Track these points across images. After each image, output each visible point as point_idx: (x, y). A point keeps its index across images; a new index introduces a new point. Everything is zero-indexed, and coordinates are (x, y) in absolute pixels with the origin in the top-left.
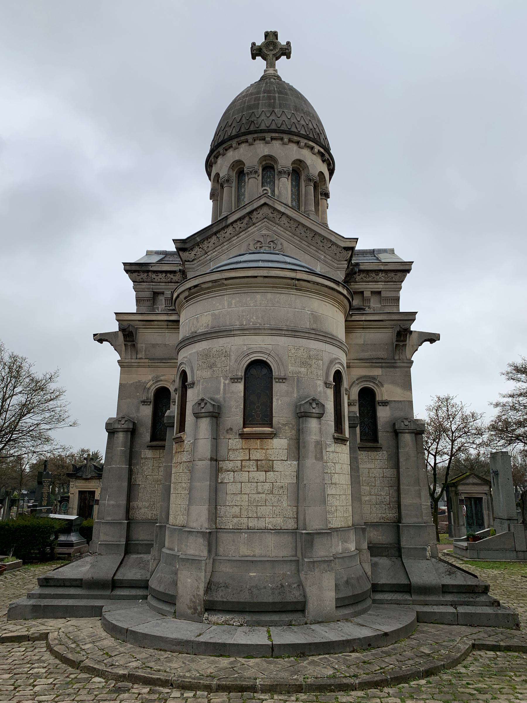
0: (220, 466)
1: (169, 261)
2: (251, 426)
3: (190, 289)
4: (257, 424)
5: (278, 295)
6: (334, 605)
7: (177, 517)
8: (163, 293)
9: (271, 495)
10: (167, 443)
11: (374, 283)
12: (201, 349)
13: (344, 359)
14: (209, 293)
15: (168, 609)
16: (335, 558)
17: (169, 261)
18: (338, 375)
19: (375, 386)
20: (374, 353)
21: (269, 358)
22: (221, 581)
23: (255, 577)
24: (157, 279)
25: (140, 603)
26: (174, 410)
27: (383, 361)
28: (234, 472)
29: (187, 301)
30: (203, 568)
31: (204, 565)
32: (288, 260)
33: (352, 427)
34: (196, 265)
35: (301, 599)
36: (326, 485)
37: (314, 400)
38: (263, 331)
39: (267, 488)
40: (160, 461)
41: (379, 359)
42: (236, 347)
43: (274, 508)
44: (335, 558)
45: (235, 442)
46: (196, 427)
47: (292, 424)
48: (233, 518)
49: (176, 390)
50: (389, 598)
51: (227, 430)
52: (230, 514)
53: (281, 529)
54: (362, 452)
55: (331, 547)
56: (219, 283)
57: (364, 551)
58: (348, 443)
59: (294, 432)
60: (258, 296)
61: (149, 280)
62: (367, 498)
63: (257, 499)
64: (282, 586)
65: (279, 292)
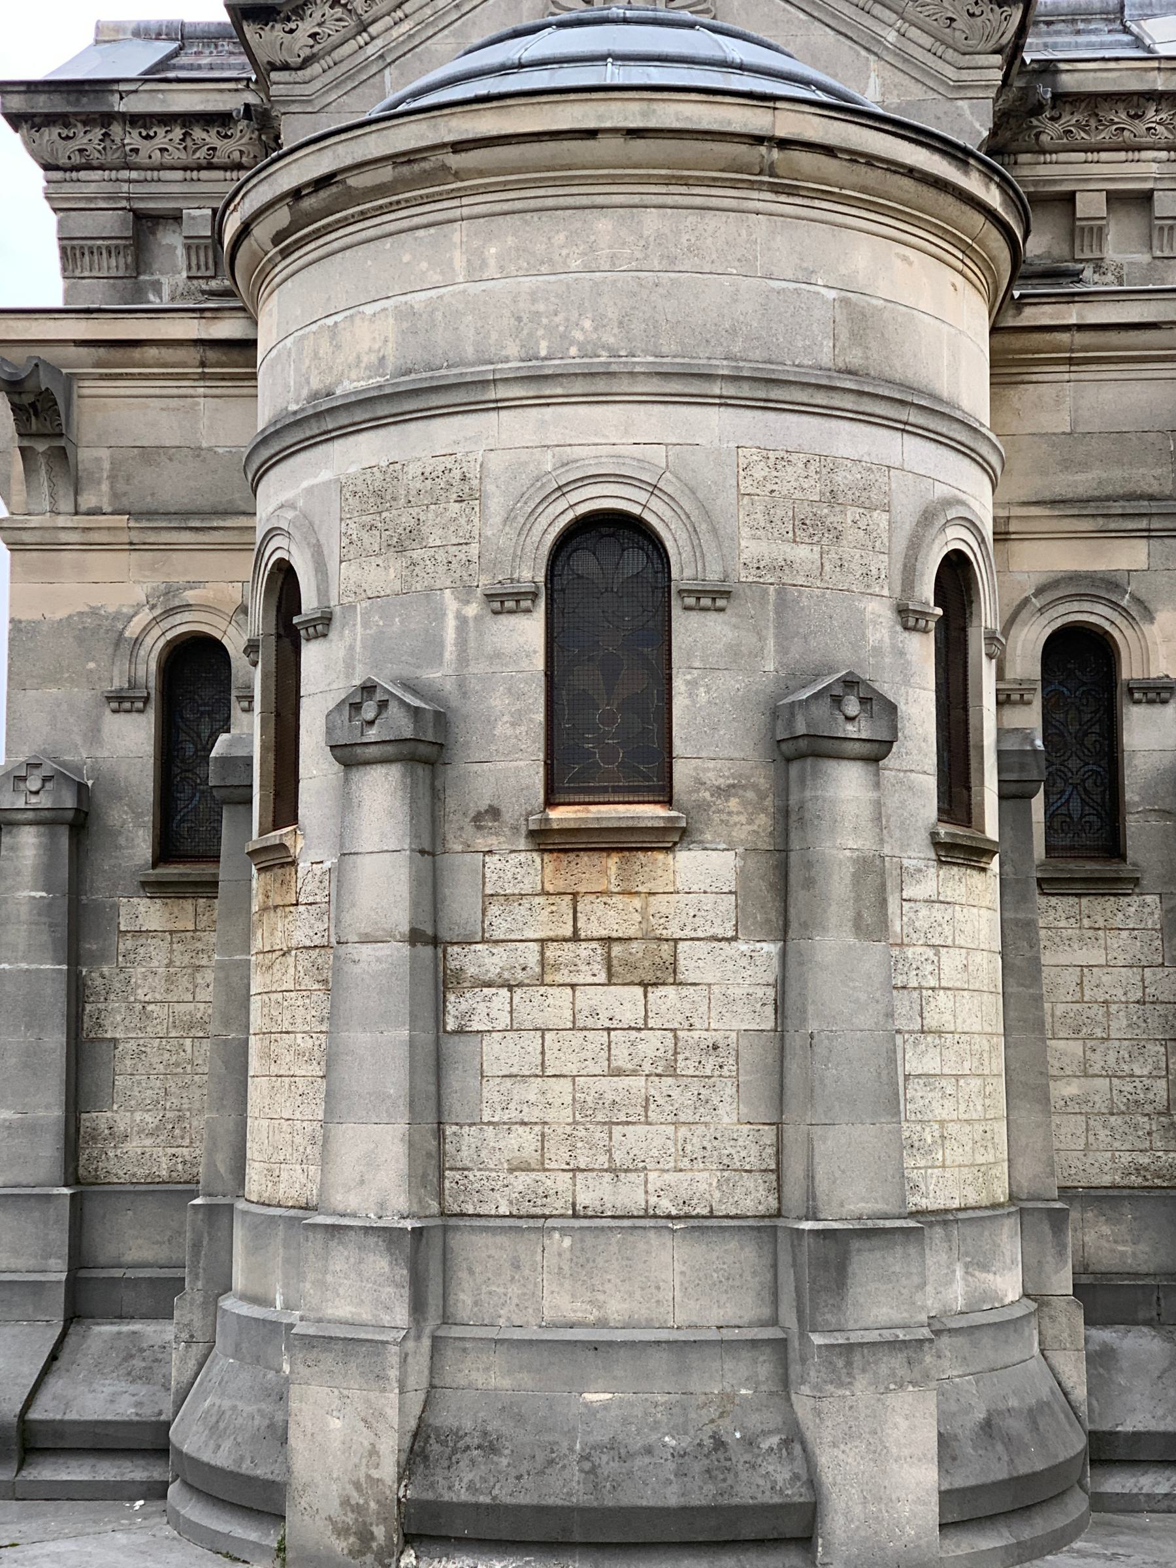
0: (453, 964)
1: (199, 67)
2: (582, 798)
3: (296, 194)
4: (605, 790)
5: (692, 218)
6: (931, 1513)
7: (277, 1168)
8: (176, 217)
9: (670, 1080)
10: (225, 871)
11: (1122, 155)
12: (352, 470)
13: (983, 505)
14: (381, 211)
15: (253, 1536)
16: (938, 1333)
17: (199, 67)
18: (956, 574)
19: (1119, 620)
20: (1117, 473)
21: (655, 504)
22: (468, 1425)
23: (606, 1407)
24: (149, 150)
25: (136, 1514)
26: (246, 733)
27: (1154, 507)
28: (510, 988)
29: (285, 253)
30: (393, 1373)
31: (394, 1360)
32: (736, 50)
33: (1013, 795)
34: (317, 84)
35: (797, 1494)
36: (899, 1039)
37: (851, 683)
38: (624, 386)
39: (651, 1053)
40: (199, 946)
41: (1141, 497)
42: (508, 456)
43: (683, 1131)
44: (938, 1333)
45: (513, 867)
46: (346, 803)
47: (755, 787)
48: (511, 1171)
49: (252, 648)
50: (1162, 1489)
51: (478, 818)
52: (496, 1159)
53: (711, 1216)
54: (1054, 901)
55: (922, 1286)
56: (425, 165)
57: (1059, 1303)
58: (995, 864)
59: (763, 821)
60: (603, 225)
61: (112, 157)
62: (1071, 1089)
63: (609, 1097)
64: (719, 1444)
65: (698, 201)
